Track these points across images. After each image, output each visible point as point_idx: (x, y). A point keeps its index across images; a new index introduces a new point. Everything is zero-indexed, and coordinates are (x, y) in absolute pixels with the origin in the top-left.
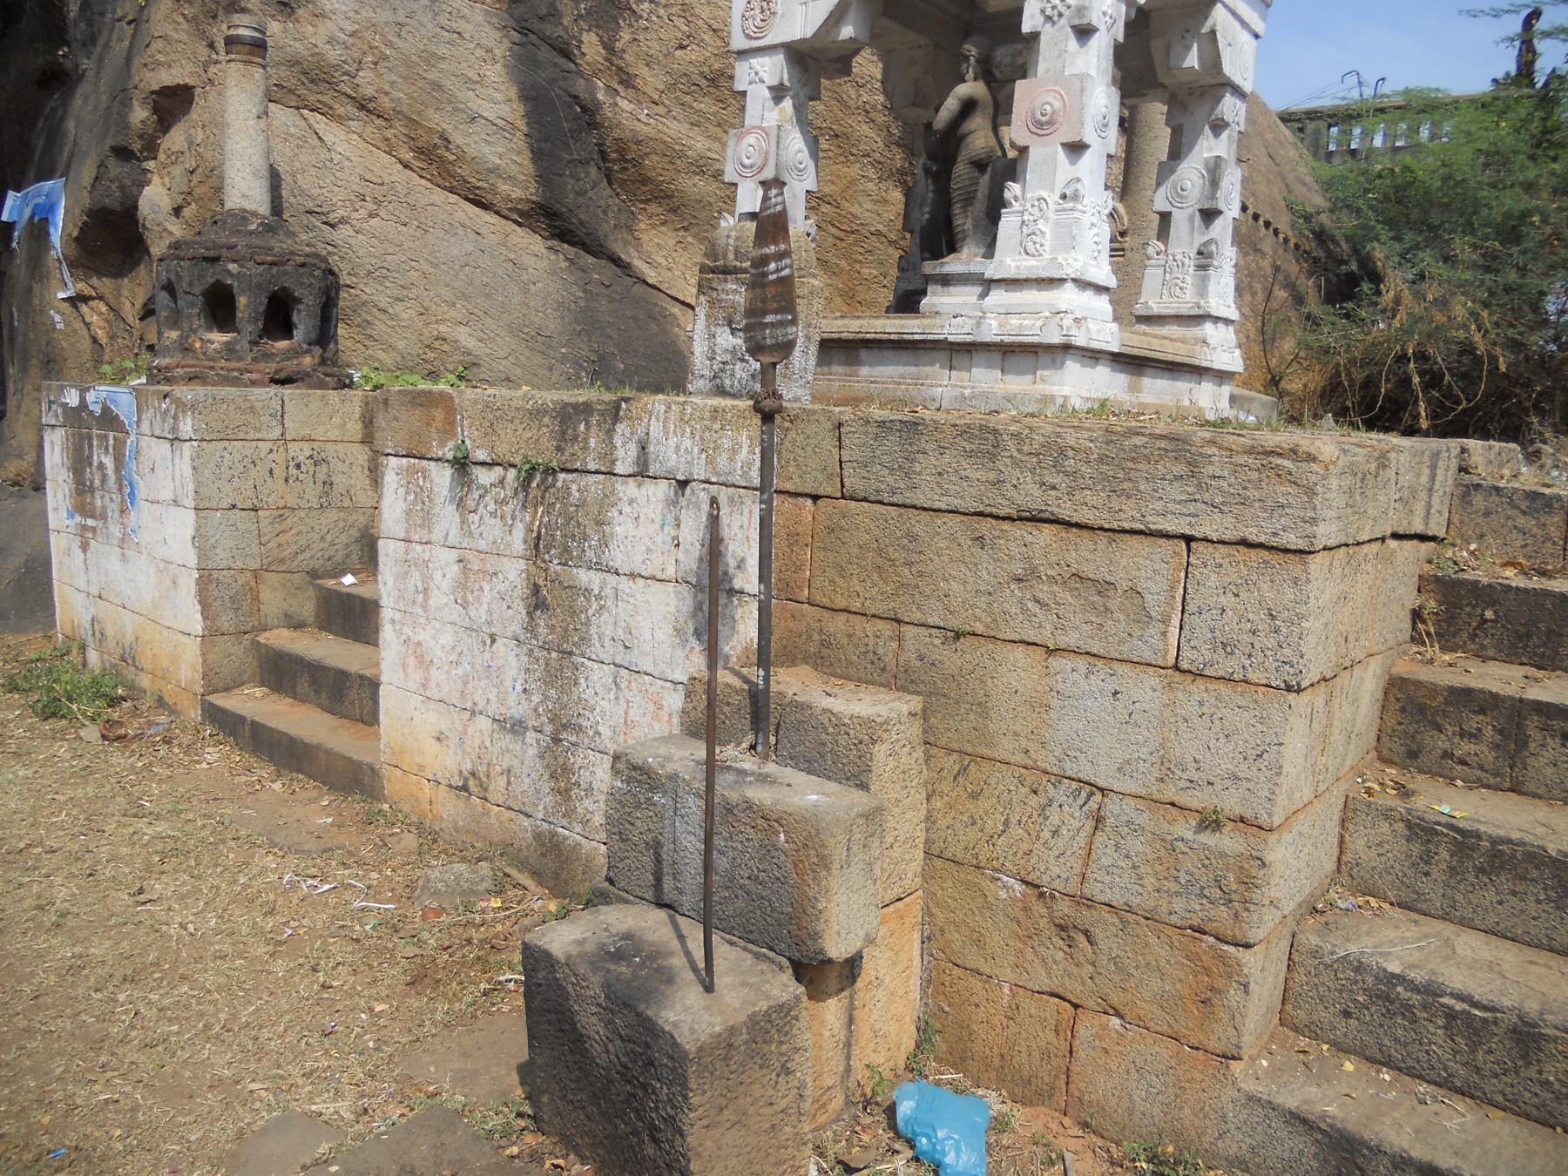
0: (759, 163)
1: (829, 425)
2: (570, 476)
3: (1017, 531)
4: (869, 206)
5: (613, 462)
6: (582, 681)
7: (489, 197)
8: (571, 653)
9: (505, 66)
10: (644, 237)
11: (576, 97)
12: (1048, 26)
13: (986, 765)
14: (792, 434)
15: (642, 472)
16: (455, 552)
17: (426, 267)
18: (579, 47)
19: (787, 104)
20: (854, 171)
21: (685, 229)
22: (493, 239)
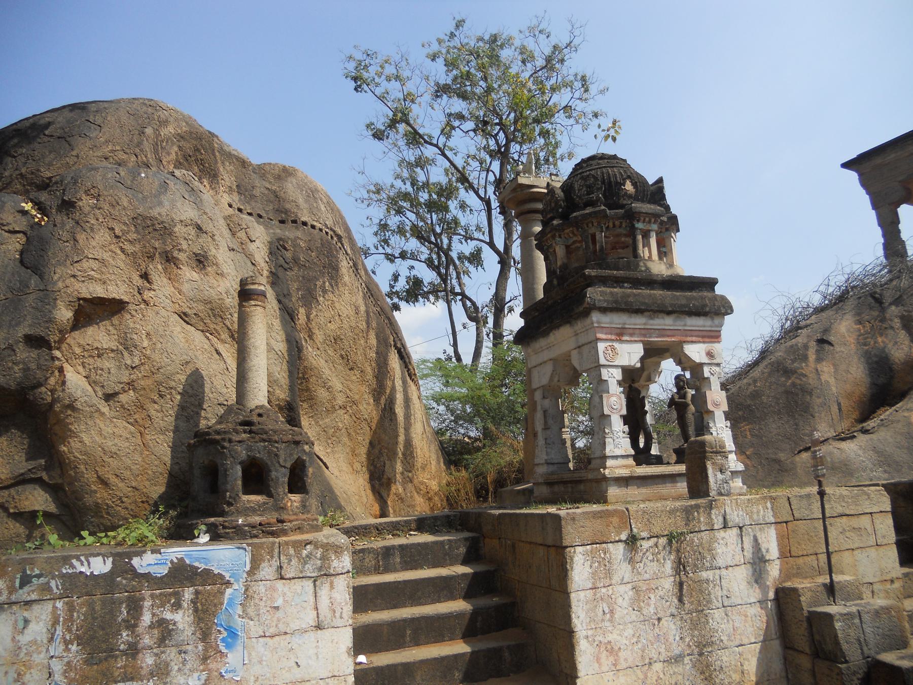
8: (702, 611)
15: (725, 526)
16: (630, 586)
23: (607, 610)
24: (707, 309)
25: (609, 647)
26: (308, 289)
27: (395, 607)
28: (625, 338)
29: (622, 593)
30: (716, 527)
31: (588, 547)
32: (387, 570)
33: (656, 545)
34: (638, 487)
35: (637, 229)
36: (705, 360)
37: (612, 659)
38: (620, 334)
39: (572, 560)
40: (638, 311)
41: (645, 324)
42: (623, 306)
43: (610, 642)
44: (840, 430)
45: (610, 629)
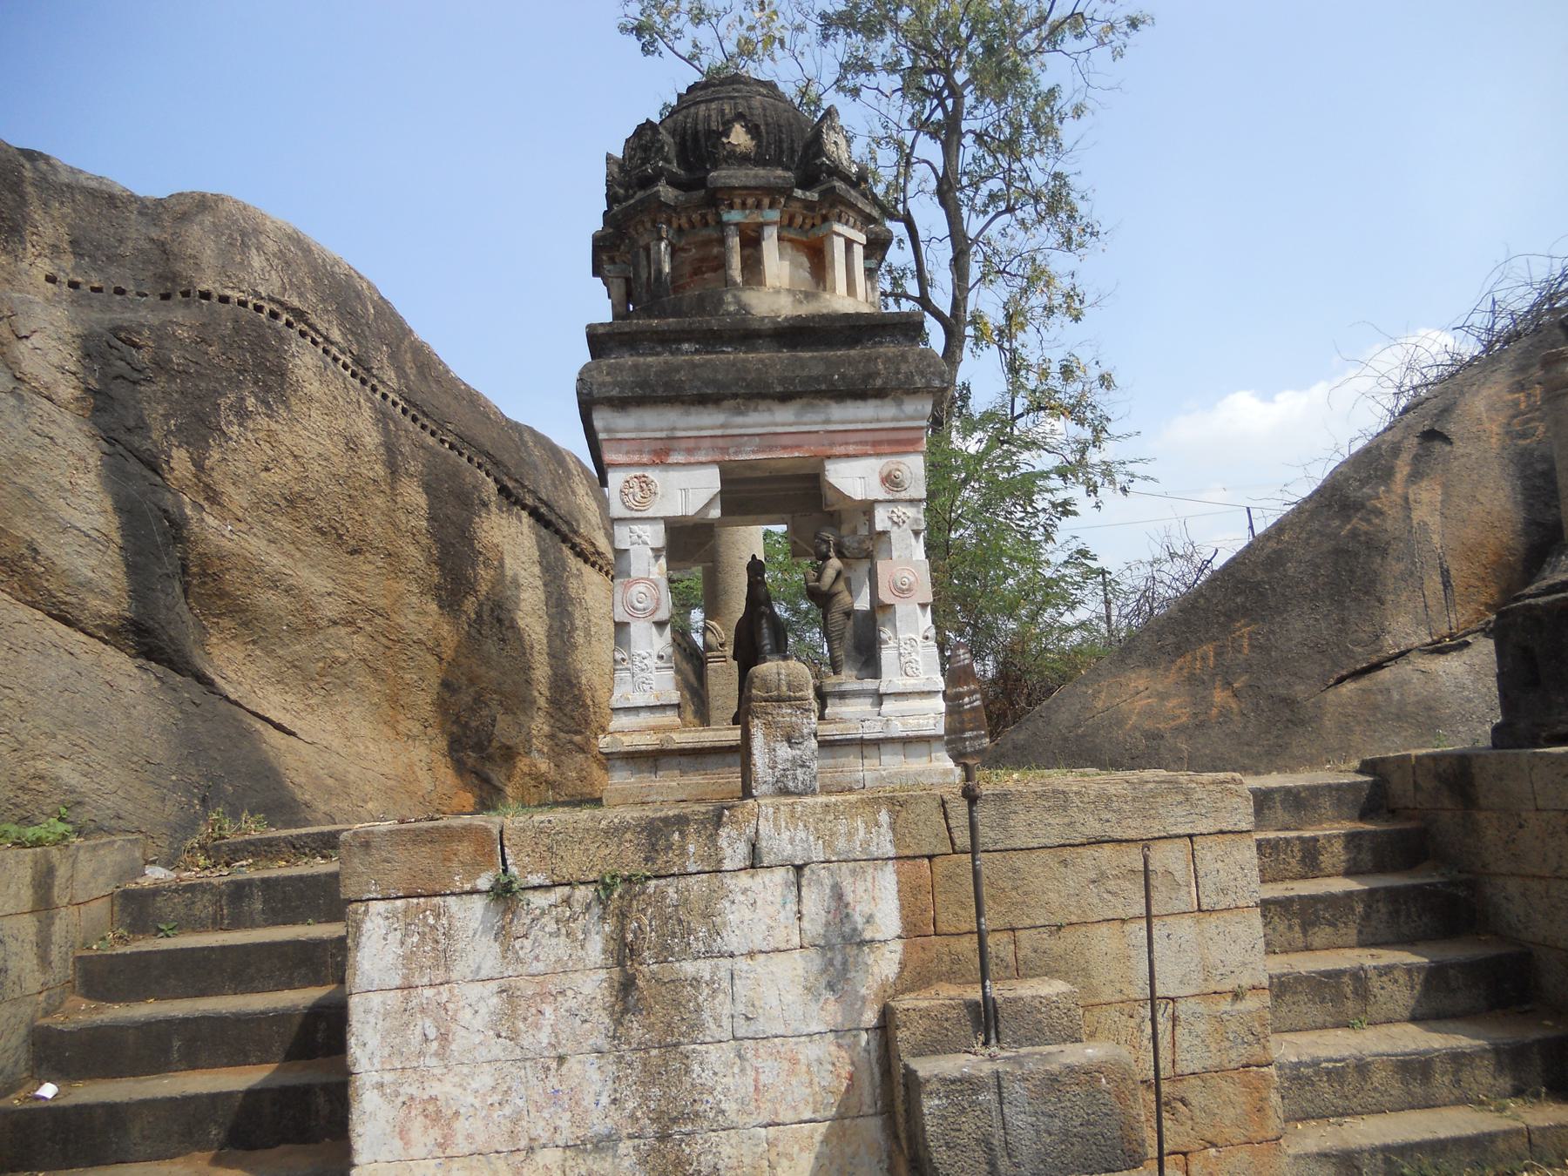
0: (652, 607)
1: (935, 804)
2: (663, 882)
3: (1087, 852)
4: (412, 617)
5: (720, 861)
6: (696, 1067)
7: (77, 612)
8: (677, 1045)
9: (99, 475)
10: (215, 652)
11: (165, 511)
12: (895, 528)
13: (1096, 1011)
14: (904, 814)
15: (755, 862)
16: (493, 986)
17: (21, 695)
18: (168, 462)
19: (663, 561)
20: (402, 586)
21: (254, 642)
22: (87, 660)
23: (432, 1033)
24: (879, 382)
25: (431, 1108)
26: (195, 414)
27: (202, 993)
28: (674, 458)
29: (473, 999)
30: (727, 865)
31: (399, 903)
32: (236, 924)
33: (567, 901)
34: (683, 773)
35: (728, 224)
36: (879, 493)
37: (436, 1133)
38: (661, 453)
39: (358, 928)
40: (703, 400)
41: (722, 426)
42: (660, 392)
43: (433, 1099)
44: (1445, 630)
45: (437, 1071)
